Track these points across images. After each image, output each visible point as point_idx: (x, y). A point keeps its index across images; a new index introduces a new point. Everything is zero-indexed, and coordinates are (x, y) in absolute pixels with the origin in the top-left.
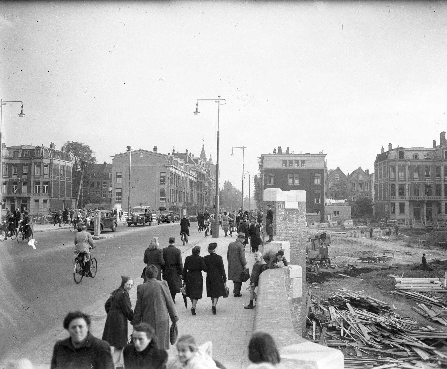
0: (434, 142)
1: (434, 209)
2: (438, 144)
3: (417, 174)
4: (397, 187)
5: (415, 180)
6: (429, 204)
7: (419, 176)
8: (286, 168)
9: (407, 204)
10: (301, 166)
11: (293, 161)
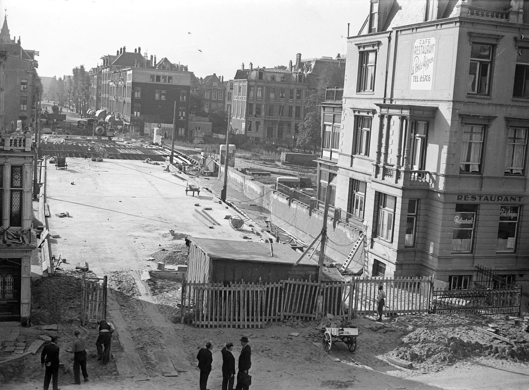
1: (285, 128)
2: (294, 64)
3: (273, 94)
4: (254, 106)
5: (271, 100)
6: (281, 124)
7: (275, 96)
8: (153, 83)
9: (262, 123)
10: (169, 82)
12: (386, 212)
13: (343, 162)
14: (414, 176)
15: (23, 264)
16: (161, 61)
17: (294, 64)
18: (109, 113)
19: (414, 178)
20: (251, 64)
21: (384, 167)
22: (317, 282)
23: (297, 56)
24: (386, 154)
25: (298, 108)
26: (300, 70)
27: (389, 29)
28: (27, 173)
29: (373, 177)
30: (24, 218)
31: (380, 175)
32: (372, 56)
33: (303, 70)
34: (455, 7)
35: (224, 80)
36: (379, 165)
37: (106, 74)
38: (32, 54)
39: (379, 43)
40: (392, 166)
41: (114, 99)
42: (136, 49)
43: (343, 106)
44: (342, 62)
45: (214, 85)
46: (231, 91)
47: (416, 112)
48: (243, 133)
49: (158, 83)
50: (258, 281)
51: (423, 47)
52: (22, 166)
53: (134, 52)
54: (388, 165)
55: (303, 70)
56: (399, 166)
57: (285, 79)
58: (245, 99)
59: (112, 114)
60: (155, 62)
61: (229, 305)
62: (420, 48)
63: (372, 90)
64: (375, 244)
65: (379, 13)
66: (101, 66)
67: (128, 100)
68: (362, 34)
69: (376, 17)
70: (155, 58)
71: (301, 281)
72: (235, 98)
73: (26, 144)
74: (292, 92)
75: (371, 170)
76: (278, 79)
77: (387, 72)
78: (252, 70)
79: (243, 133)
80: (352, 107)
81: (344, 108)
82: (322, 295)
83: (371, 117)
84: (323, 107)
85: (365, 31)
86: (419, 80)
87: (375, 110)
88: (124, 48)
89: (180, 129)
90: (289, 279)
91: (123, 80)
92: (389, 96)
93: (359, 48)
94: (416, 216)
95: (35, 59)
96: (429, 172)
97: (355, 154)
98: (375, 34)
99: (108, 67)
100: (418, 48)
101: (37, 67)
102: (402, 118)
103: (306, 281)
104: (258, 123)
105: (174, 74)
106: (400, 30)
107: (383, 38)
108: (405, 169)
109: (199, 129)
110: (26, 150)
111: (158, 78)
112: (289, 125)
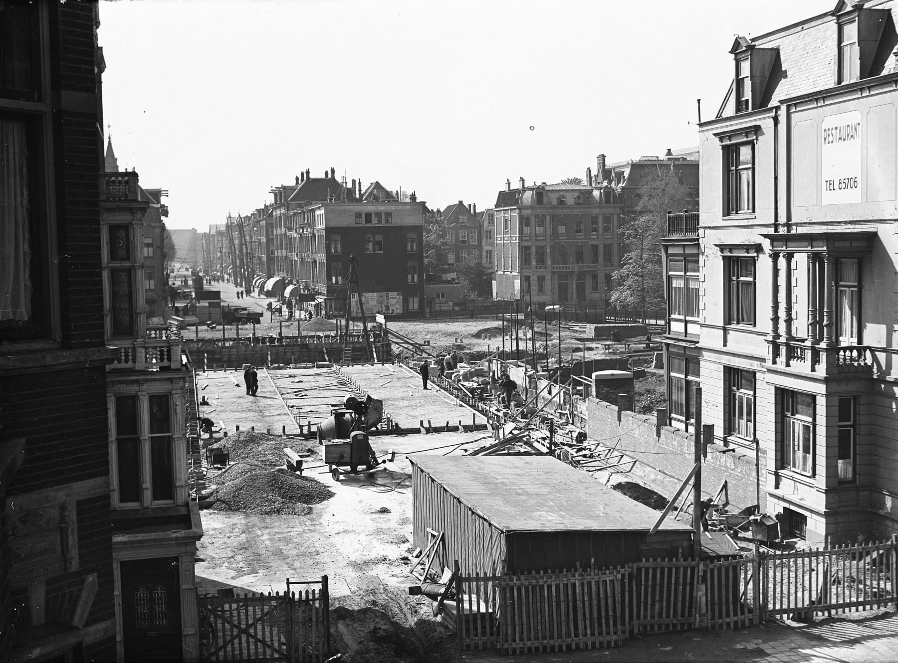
0: (589, 171)
2: (594, 172)
3: (564, 227)
6: (581, 275)
7: (567, 230)
9: (548, 277)
11: (371, 214)
12: (799, 421)
13: (710, 339)
14: (845, 356)
15: (183, 567)
16: (369, 188)
17: (594, 172)
18: (290, 283)
19: (845, 359)
20: (522, 180)
21: (787, 345)
22: (693, 560)
23: (598, 160)
24: (789, 321)
25: (608, 248)
26: (605, 183)
27: (773, 103)
28: (176, 405)
29: (769, 364)
30: (178, 484)
31: (782, 359)
32: (745, 153)
33: (610, 182)
34: (892, 55)
35: (477, 211)
36: (778, 341)
37: (280, 217)
38: (156, 194)
39: (757, 130)
40: (803, 341)
41: (296, 259)
42: (327, 172)
43: (700, 242)
44: (676, 163)
45: (461, 221)
46: (490, 228)
47: (837, 244)
48: (518, 298)
49: (369, 225)
50: (589, 566)
51: (838, 130)
52: (167, 395)
53: (323, 176)
54: (794, 339)
55: (610, 182)
56: (817, 341)
57: (581, 201)
58: (516, 240)
59: (295, 283)
60: (360, 191)
61: (543, 611)
62: (834, 131)
63: (750, 211)
64: (784, 482)
65: (752, 77)
66: (272, 205)
67: (321, 257)
68: (724, 115)
69: (748, 84)
70: (360, 183)
71: (664, 561)
72: (499, 238)
73: (173, 356)
74: (595, 220)
75: (766, 351)
76: (570, 200)
77: (776, 178)
78: (524, 189)
79: (518, 298)
80: (718, 242)
81: (702, 246)
82: (703, 582)
83: (754, 257)
84: (664, 245)
85: (730, 110)
86: (836, 186)
87: (760, 245)
88: (308, 172)
89: (411, 300)
90: (644, 560)
91: (309, 225)
92: (783, 219)
93: (721, 140)
94: (854, 426)
95: (162, 203)
96: (869, 348)
97: (730, 324)
98: (750, 115)
99: (284, 205)
100: (830, 132)
101: (167, 216)
102: (815, 257)
103: (674, 559)
104: (541, 279)
105: (394, 208)
106: (793, 103)
107: (766, 123)
108: (827, 346)
109: (443, 296)
110: (172, 367)
111: (368, 216)
112: (595, 277)
